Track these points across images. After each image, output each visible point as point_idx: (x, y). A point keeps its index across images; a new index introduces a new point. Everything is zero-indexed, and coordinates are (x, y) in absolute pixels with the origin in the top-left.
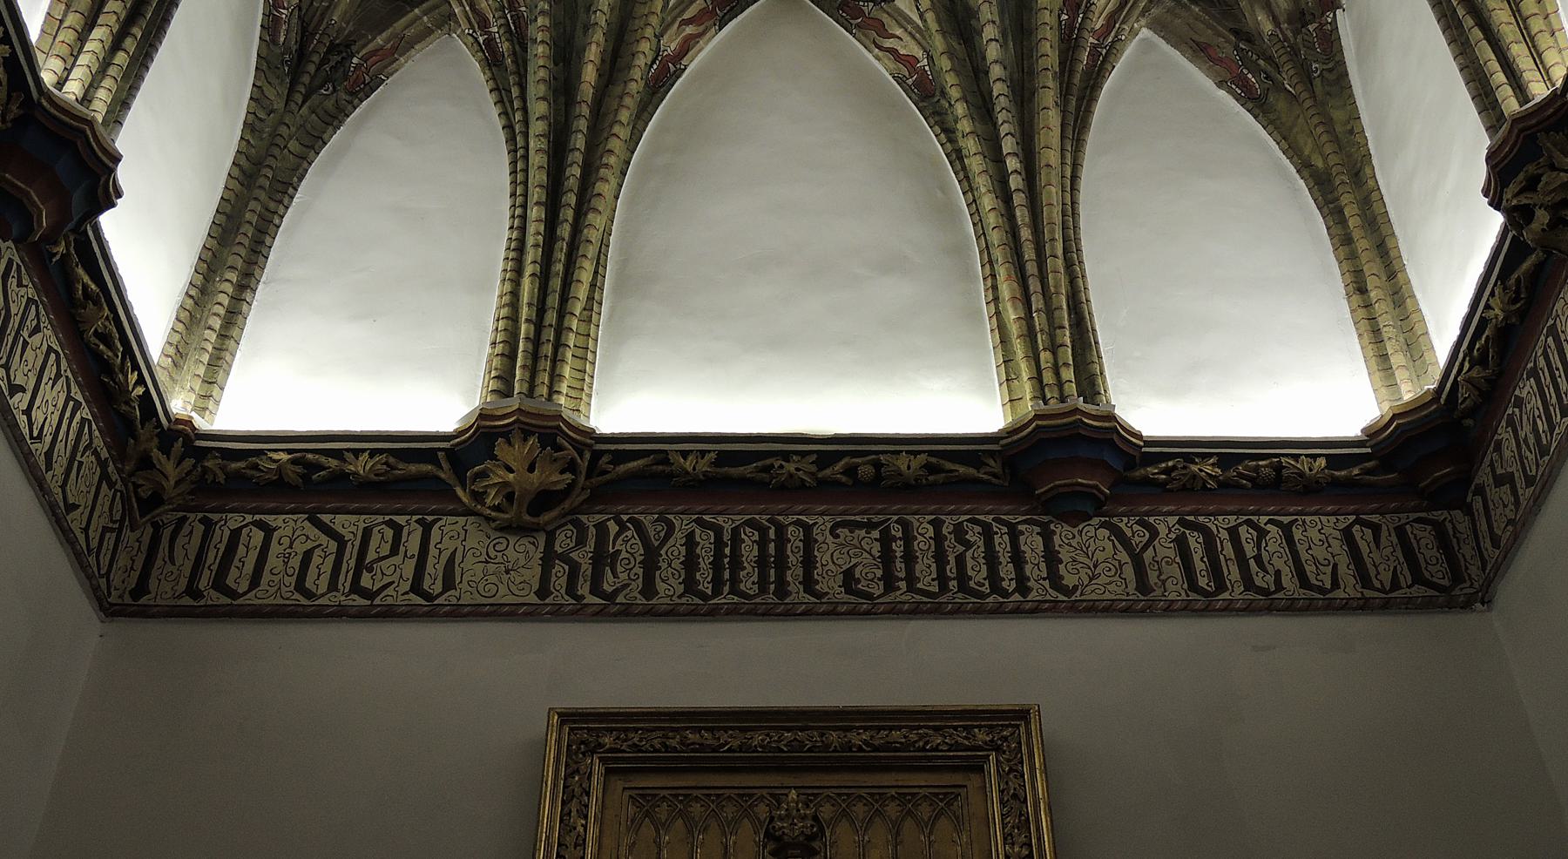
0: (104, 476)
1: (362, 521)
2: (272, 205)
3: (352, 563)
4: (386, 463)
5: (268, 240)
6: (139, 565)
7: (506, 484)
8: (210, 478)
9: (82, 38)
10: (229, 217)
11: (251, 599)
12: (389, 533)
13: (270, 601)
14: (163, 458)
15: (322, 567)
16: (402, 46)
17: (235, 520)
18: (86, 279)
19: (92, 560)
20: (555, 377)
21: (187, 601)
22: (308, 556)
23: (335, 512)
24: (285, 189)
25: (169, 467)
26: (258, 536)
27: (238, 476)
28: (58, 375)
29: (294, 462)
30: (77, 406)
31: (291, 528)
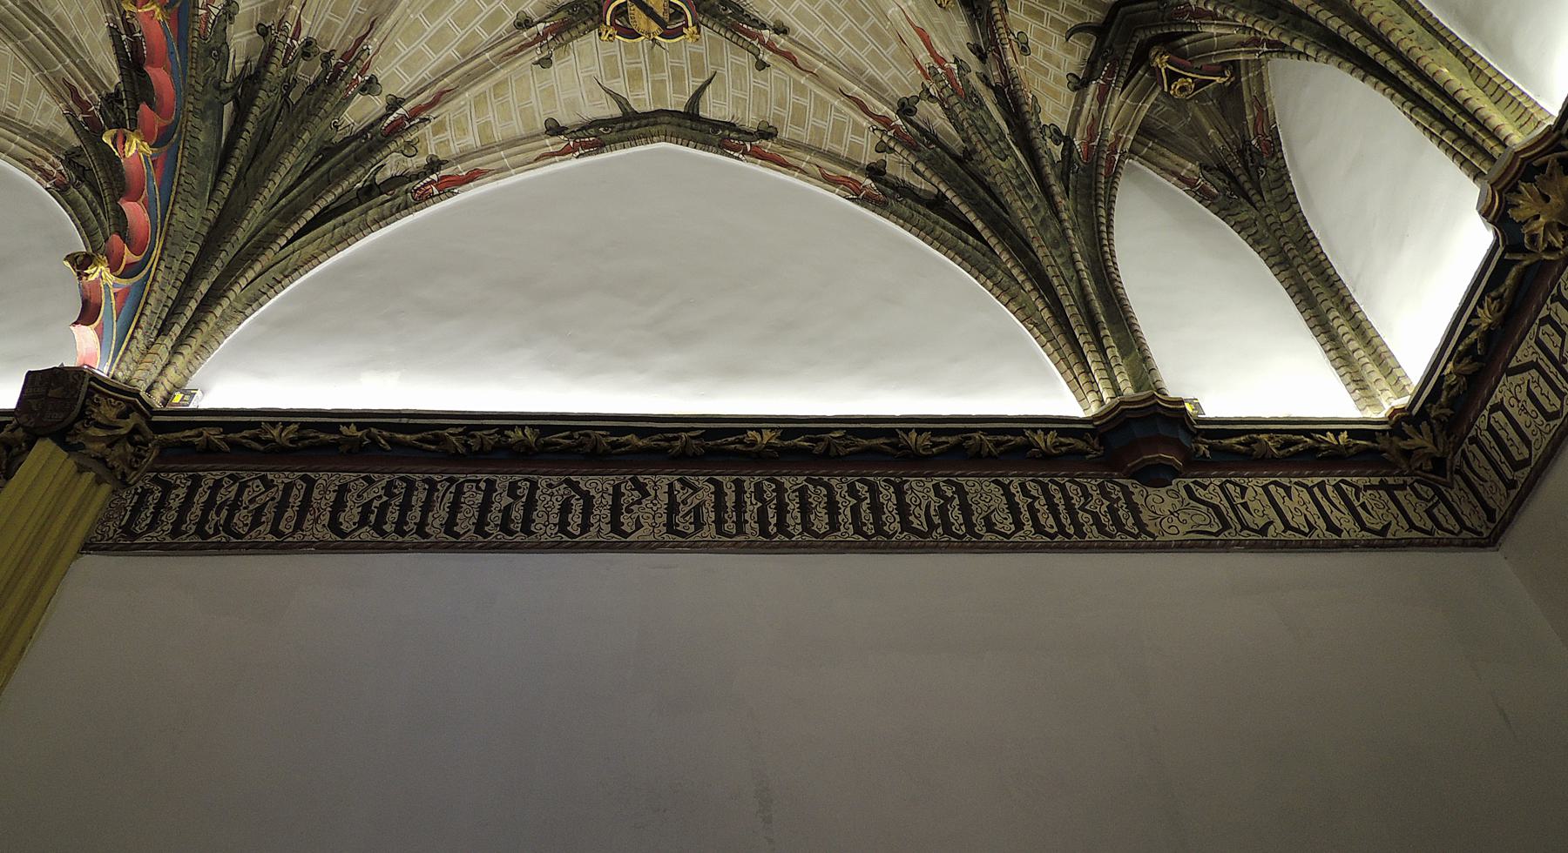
0: (1390, 489)
1: (1529, 340)
2: (1312, 255)
3: (1554, 369)
4: (1493, 299)
5: (1330, 272)
6: (1475, 501)
7: (1548, 226)
8: (1444, 418)
9: (1088, 371)
10: (1300, 292)
11: (1537, 454)
12: (1548, 328)
13: (1545, 443)
14: (1410, 442)
15: (1542, 390)
16: (1261, 102)
17: (1482, 422)
18: (1234, 440)
19: (1439, 534)
20: (1493, 134)
21: (1513, 493)
22: (1530, 394)
23: (1513, 354)
24: (1306, 240)
25: (1418, 441)
26: (1499, 415)
27: (1451, 403)
28: (1287, 490)
29: (1458, 362)
30: (1321, 486)
31: (1507, 390)
